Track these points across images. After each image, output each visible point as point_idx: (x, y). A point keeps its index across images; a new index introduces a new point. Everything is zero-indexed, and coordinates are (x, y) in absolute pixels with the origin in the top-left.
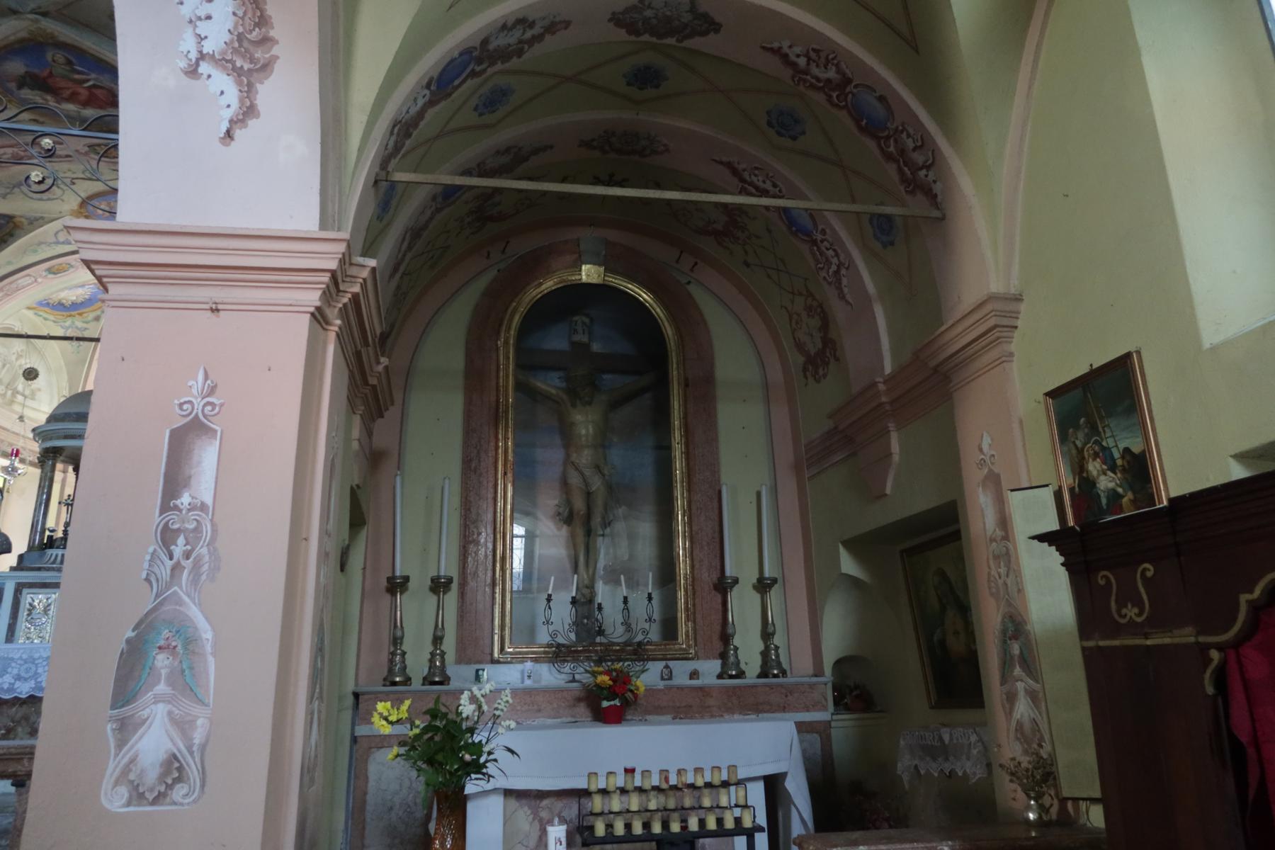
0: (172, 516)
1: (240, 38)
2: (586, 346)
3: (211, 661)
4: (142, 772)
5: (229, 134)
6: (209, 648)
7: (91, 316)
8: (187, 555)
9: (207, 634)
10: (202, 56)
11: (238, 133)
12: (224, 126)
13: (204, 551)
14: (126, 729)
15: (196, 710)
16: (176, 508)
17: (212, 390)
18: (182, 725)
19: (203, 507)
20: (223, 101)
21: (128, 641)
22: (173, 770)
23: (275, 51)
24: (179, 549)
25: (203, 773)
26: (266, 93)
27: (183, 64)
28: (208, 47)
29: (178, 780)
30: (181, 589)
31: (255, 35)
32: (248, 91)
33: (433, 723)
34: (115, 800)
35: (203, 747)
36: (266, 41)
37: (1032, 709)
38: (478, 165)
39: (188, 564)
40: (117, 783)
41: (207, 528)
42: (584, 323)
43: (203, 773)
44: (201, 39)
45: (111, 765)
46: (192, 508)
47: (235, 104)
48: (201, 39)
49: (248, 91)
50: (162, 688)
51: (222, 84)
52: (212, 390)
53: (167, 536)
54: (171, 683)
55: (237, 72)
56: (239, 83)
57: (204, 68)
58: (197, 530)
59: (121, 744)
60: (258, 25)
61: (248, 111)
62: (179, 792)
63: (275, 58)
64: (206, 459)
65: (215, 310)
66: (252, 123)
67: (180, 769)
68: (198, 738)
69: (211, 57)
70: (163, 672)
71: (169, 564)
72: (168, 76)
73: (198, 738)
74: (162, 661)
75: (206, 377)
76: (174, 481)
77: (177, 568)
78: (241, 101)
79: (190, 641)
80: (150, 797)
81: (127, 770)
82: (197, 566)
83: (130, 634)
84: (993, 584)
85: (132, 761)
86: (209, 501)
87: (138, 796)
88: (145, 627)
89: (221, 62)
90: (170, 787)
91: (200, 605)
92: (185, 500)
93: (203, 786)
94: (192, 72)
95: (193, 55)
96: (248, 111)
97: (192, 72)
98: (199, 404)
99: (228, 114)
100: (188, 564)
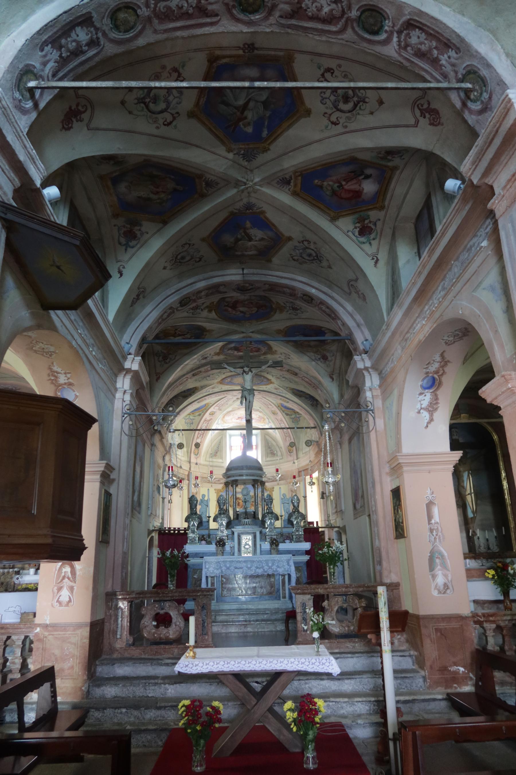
0: (431, 525)
1: (431, 403)
2: (458, 440)
3: (448, 561)
4: (439, 587)
5: (427, 426)
6: (447, 558)
7: (197, 414)
8: (437, 535)
9: (446, 554)
10: (421, 408)
11: (429, 425)
12: (425, 425)
13: (440, 534)
14: (434, 577)
15: (448, 572)
16: (431, 524)
17: (433, 493)
18: (445, 576)
19: (437, 523)
20: (426, 418)
21: (429, 556)
22: (446, 586)
23: (439, 405)
24: (435, 533)
25: (452, 586)
26: (436, 415)
27: (417, 411)
28: (423, 406)
29: (448, 588)
30: (437, 543)
31: (435, 402)
32: (431, 415)
33: (145, 639)
34: (435, 593)
35: (451, 581)
36: (437, 403)
37: (438, 33)
38: (69, 129)
39: (437, 537)
40: (435, 589)
41: (440, 528)
42: (456, 431)
43: (452, 586)
44: (421, 404)
45: (432, 585)
46: (435, 523)
47: (428, 418)
48: (421, 404)
49: (431, 415)
50: (439, 567)
51: (426, 415)
52: (433, 493)
53: (431, 531)
54: (441, 566)
55: (429, 411)
56: (429, 414)
57: (422, 411)
58: (438, 529)
59: (434, 580)
60: (436, 400)
61: (431, 420)
62: (448, 591)
63: (439, 407)
64: (435, 511)
65: (429, 472)
66: (432, 423)
67: (447, 586)
68: (450, 578)
69: (423, 409)
70: (439, 564)
71: (433, 537)
72: (413, 414)
73: (450, 578)
74: (438, 561)
75: (430, 490)
76: (430, 517)
77: (435, 538)
78: (430, 418)
79: (443, 556)
80: (442, 592)
81: (436, 586)
82: (439, 538)
83: (429, 555)
84: (478, 249)
85: (437, 584)
86: (438, 521)
87: (440, 592)
88: (432, 553)
89: (426, 409)
90: (446, 590)
91: (442, 547)
92: (433, 521)
93: (453, 590)
94: (419, 412)
95: (419, 409)
96: (431, 420)
97: (419, 412)
98: (430, 497)
99: (426, 421)
100: (437, 537)
